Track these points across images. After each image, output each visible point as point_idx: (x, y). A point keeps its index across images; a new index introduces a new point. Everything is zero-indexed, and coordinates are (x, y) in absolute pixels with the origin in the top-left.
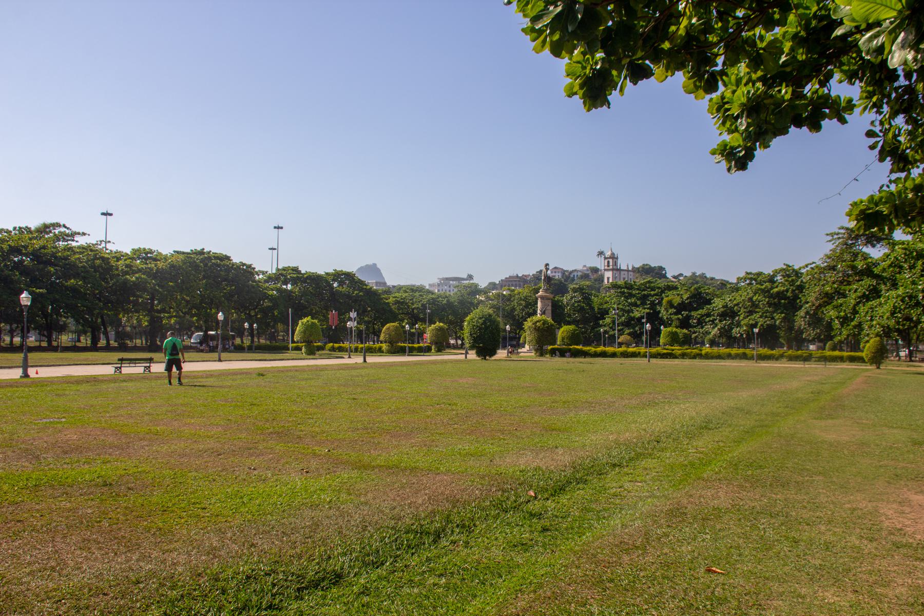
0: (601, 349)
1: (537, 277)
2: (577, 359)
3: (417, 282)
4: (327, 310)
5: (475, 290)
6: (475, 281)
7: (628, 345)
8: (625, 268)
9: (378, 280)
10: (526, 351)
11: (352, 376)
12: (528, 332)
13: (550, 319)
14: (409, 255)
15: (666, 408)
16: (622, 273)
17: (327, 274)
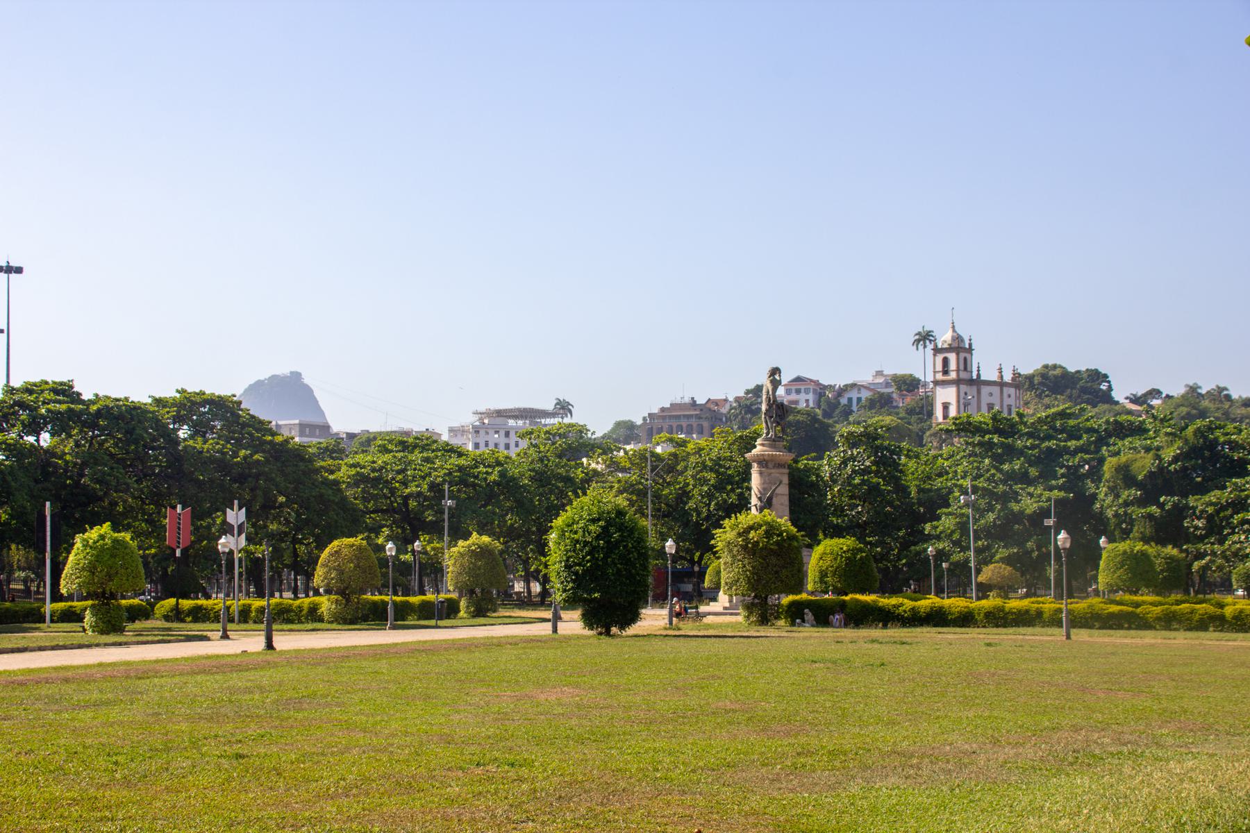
0: (929, 602)
1: (747, 407)
2: (864, 632)
3: (415, 422)
4: (159, 505)
5: (576, 445)
6: (577, 418)
7: (1006, 590)
8: (994, 377)
9: (311, 419)
10: (722, 610)
11: (232, 691)
12: (725, 558)
13: (784, 522)
14: (392, 351)
15: (1127, 770)
16: (985, 390)
17: (159, 402)
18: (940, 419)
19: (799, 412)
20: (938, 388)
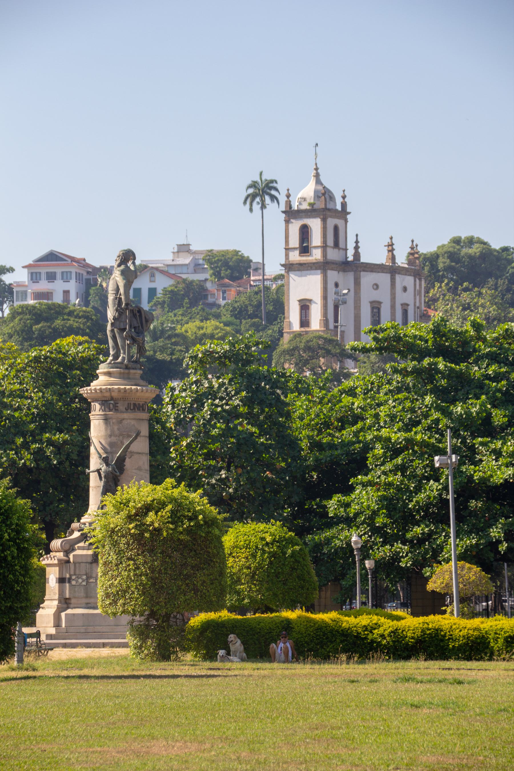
8: (381, 258)
16: (368, 279)
18: (296, 327)
19: (71, 313)
20: (292, 275)
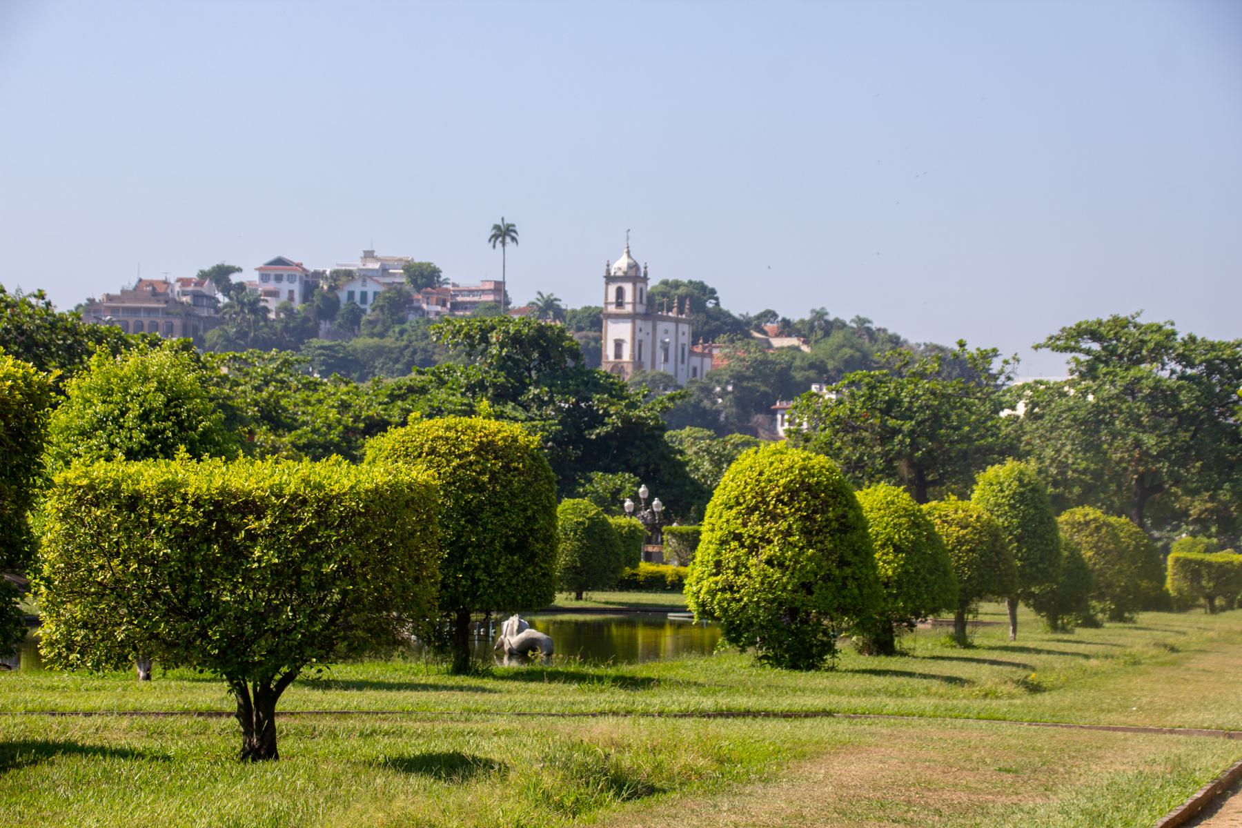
18: (611, 358)
